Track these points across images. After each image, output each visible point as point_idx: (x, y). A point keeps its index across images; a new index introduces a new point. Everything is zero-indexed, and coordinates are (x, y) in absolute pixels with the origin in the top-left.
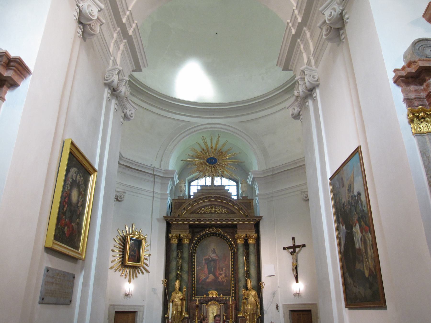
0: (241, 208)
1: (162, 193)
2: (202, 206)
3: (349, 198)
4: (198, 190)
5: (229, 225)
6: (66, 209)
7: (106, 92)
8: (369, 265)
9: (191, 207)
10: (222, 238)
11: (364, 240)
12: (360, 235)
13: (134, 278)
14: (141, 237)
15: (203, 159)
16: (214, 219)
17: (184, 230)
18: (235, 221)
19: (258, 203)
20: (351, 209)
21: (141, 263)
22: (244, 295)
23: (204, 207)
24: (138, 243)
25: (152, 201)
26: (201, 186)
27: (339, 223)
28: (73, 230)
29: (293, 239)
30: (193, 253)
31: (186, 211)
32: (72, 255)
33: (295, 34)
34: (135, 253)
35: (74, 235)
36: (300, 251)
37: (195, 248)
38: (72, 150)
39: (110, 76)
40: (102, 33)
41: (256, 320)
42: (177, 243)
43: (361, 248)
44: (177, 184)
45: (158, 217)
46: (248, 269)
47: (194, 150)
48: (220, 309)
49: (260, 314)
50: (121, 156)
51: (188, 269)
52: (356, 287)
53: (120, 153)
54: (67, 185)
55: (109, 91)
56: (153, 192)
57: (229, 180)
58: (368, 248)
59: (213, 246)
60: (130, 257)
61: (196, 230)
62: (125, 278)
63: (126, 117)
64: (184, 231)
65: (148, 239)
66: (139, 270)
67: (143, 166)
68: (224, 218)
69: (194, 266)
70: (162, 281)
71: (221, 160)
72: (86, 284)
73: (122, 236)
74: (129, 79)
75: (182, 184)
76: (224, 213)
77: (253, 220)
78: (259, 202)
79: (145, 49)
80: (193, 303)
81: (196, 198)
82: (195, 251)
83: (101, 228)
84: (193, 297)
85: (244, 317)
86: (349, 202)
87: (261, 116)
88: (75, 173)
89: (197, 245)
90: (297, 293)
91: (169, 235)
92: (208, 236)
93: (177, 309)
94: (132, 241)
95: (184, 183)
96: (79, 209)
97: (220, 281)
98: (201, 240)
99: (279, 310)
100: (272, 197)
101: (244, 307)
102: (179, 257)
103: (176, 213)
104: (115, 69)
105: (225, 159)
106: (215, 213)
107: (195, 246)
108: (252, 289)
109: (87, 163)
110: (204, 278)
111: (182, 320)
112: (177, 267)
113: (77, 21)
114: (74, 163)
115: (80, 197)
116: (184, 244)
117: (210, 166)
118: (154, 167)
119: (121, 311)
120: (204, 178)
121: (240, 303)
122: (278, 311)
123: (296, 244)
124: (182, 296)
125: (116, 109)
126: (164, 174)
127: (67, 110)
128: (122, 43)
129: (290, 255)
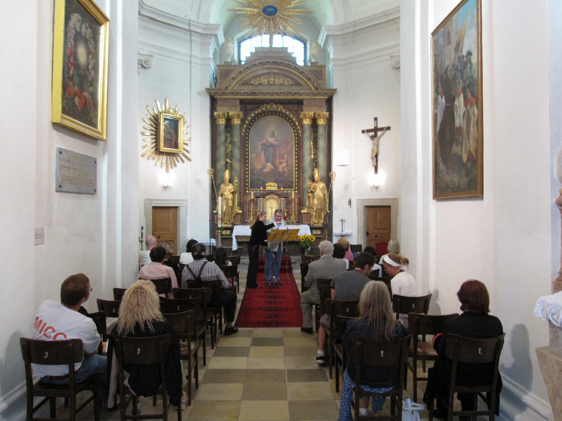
3: (455, 58)
4: (251, 53)
8: (470, 148)
9: (242, 76)
10: (283, 118)
11: (467, 116)
12: (463, 109)
13: (172, 168)
14: (178, 116)
15: (258, 9)
16: (273, 93)
18: (301, 95)
19: (332, 71)
20: (455, 75)
22: (310, 188)
23: (260, 76)
24: (174, 124)
27: (438, 94)
28: (86, 101)
29: (376, 119)
30: (246, 136)
34: (171, 136)
36: (383, 134)
41: (323, 216)
42: (225, 123)
43: (462, 126)
46: (316, 156)
48: (280, 203)
49: (329, 210)
51: (241, 157)
52: (449, 174)
56: (191, 55)
58: (471, 127)
60: (166, 141)
61: (250, 107)
62: (161, 167)
64: (234, 108)
65: (187, 118)
66: (178, 158)
69: (247, 153)
72: (111, 170)
76: (286, 84)
77: (324, 93)
78: (333, 70)
80: (247, 197)
82: (249, 134)
83: (123, 91)
84: (246, 190)
85: (309, 213)
86: (454, 65)
88: (79, 21)
89: (251, 126)
90: (375, 187)
91: (214, 113)
92: (265, 115)
93: (227, 204)
95: (231, 42)
99: (351, 206)
100: (351, 63)
101: (309, 202)
107: (248, 128)
110: (260, 167)
111: (234, 217)
112: (226, 154)
115: (90, 56)
116: (234, 125)
119: (160, 206)
121: (304, 197)
122: (351, 207)
123: (379, 126)
124: (233, 188)
126: (205, 29)
129: (370, 140)
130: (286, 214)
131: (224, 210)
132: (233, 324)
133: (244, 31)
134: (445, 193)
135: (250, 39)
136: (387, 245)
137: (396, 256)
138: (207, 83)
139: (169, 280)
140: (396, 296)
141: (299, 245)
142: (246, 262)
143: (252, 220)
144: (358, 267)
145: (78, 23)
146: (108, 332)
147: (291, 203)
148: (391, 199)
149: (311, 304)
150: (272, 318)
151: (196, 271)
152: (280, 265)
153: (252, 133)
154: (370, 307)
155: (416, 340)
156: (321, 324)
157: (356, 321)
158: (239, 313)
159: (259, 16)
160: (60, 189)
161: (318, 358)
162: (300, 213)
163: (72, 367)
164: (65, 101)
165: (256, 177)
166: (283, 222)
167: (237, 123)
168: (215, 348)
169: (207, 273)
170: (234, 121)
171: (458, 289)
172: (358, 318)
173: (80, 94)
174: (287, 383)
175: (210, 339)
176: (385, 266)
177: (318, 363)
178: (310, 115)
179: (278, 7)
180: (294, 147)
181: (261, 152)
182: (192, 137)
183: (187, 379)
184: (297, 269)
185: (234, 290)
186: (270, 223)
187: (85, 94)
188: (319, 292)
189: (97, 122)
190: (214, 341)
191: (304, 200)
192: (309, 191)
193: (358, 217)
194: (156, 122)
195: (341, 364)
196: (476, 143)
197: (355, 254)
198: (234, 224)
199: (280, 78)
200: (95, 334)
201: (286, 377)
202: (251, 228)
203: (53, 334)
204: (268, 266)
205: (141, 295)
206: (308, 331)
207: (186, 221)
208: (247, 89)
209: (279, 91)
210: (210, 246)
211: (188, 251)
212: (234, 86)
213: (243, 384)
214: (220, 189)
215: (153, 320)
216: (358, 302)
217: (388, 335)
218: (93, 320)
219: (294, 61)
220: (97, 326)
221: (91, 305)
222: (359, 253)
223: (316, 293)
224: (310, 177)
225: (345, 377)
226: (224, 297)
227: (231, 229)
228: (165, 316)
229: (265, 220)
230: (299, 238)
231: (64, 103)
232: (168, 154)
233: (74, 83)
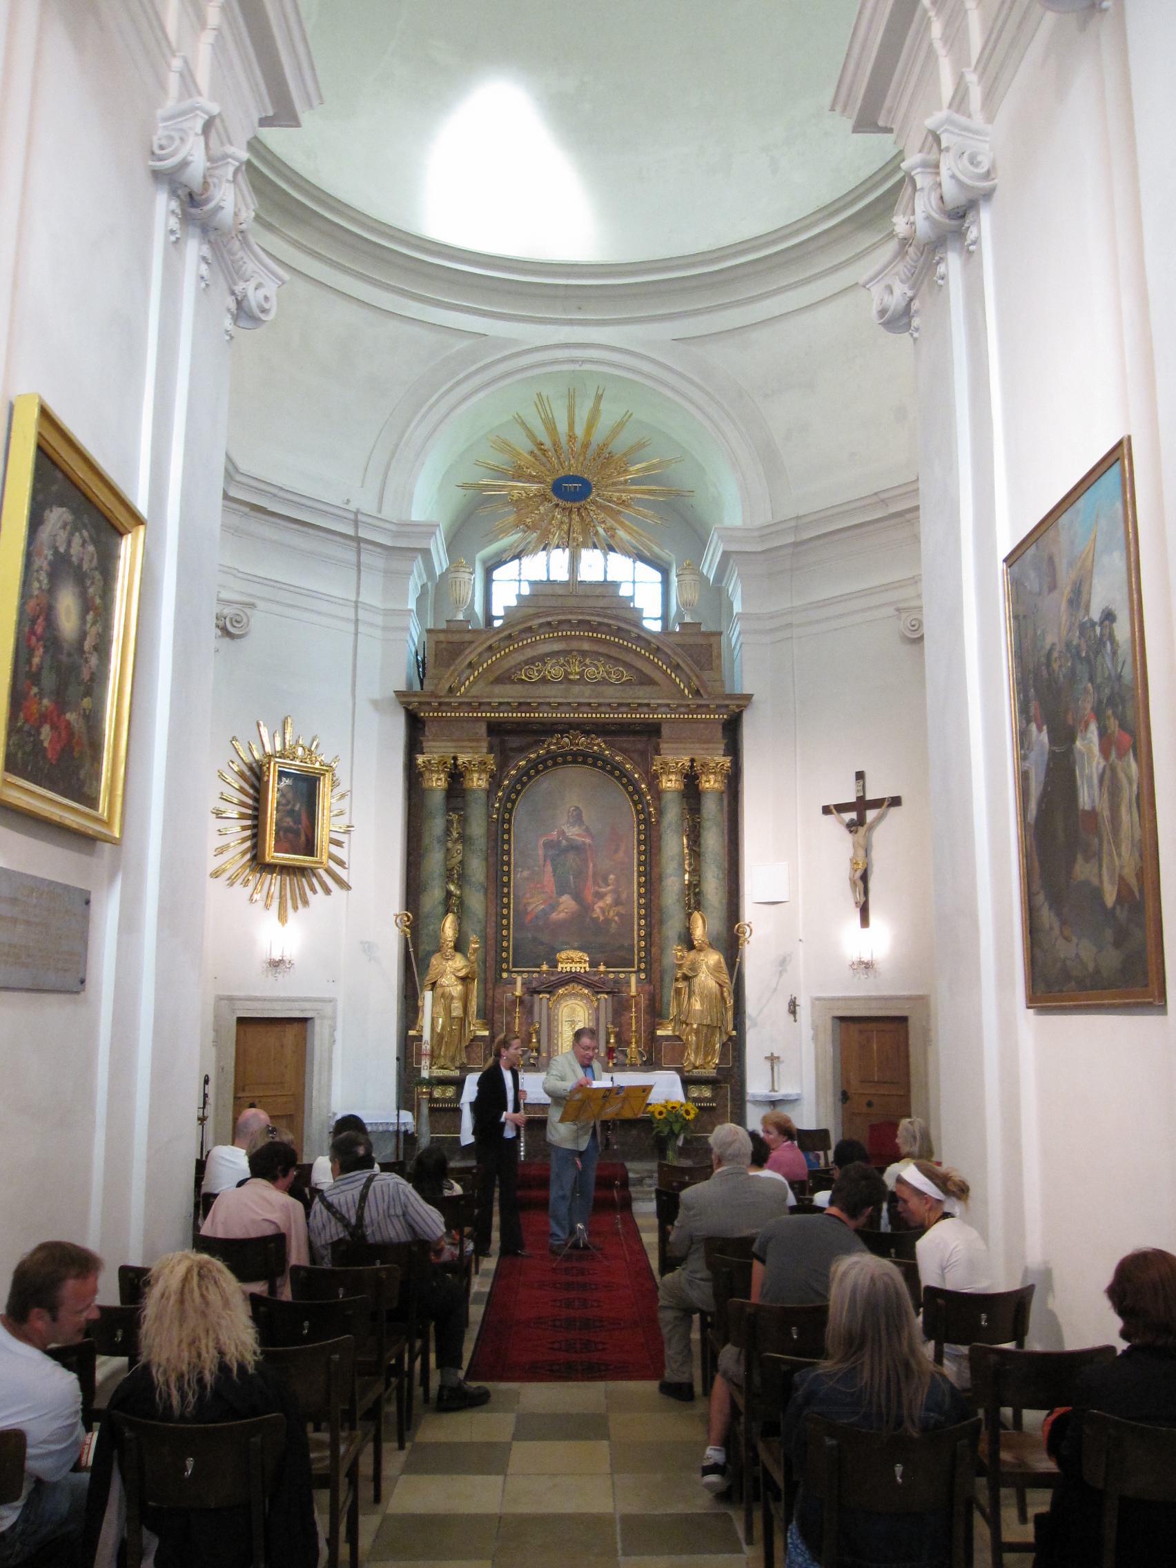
0: (678, 665)
4: (519, 596)
6: (41, 664)
7: (163, 206)
11: (1110, 782)
12: (1098, 763)
13: (296, 908)
14: (317, 765)
16: (580, 704)
18: (654, 711)
19: (738, 647)
20: (1073, 671)
21: (322, 855)
22: (680, 966)
23: (542, 658)
28: (71, 734)
29: (860, 776)
32: (75, 826)
34: (297, 821)
35: (76, 754)
36: (879, 819)
38: (45, 439)
39: (171, 138)
41: (718, 1046)
42: (446, 785)
43: (1098, 809)
46: (697, 878)
47: (504, 446)
49: (735, 1028)
52: (1067, 939)
54: (37, 571)
56: (356, 602)
59: (573, 799)
60: (281, 833)
61: (514, 742)
62: (267, 907)
63: (243, 312)
65: (341, 771)
66: (314, 881)
69: (506, 868)
70: (397, 916)
72: (129, 924)
73: (247, 761)
77: (718, 706)
80: (505, 992)
86: (1068, 645)
88: (64, 527)
89: (518, 793)
92: (555, 764)
93: (448, 1010)
95: (468, 570)
97: (598, 917)
100: (790, 625)
101: (679, 1005)
102: (455, 835)
103: (440, 679)
105: (621, 483)
106: (581, 681)
107: (509, 799)
110: (543, 907)
111: (466, 1047)
114: (54, 488)
115: (90, 617)
116: (474, 791)
117: (564, 509)
121: (665, 991)
122: (795, 1021)
123: (869, 797)
125: (202, 278)
126: (397, 535)
129: (844, 832)
131: (439, 1029)
133: (502, 538)
135: (517, 560)
138: (399, 676)
140: (933, 1292)
145: (61, 532)
148: (909, 998)
149: (687, 1311)
152: (592, 1187)
153: (520, 814)
154: (861, 1346)
155: (995, 1422)
159: (542, 503)
161: (707, 1470)
162: (653, 1040)
164: (15, 738)
168: (408, 1445)
170: (472, 779)
171: (1107, 1276)
173: (56, 719)
174: (621, 1559)
175: (394, 1419)
178: (680, 764)
179: (593, 480)
180: (635, 851)
182: (353, 824)
184: (643, 1200)
187: (71, 716)
189: (99, 792)
190: (405, 1427)
191: (665, 1000)
192: (679, 975)
194: (256, 783)
196: (1137, 855)
199: (599, 664)
201: (619, 1539)
206: (679, 1392)
207: (330, 1059)
208: (510, 693)
210: (398, 1132)
212: (473, 684)
219: (635, 617)
223: (702, 1279)
224: (679, 937)
230: (650, 1108)
231: (11, 743)
232: (285, 870)
233: (41, 690)
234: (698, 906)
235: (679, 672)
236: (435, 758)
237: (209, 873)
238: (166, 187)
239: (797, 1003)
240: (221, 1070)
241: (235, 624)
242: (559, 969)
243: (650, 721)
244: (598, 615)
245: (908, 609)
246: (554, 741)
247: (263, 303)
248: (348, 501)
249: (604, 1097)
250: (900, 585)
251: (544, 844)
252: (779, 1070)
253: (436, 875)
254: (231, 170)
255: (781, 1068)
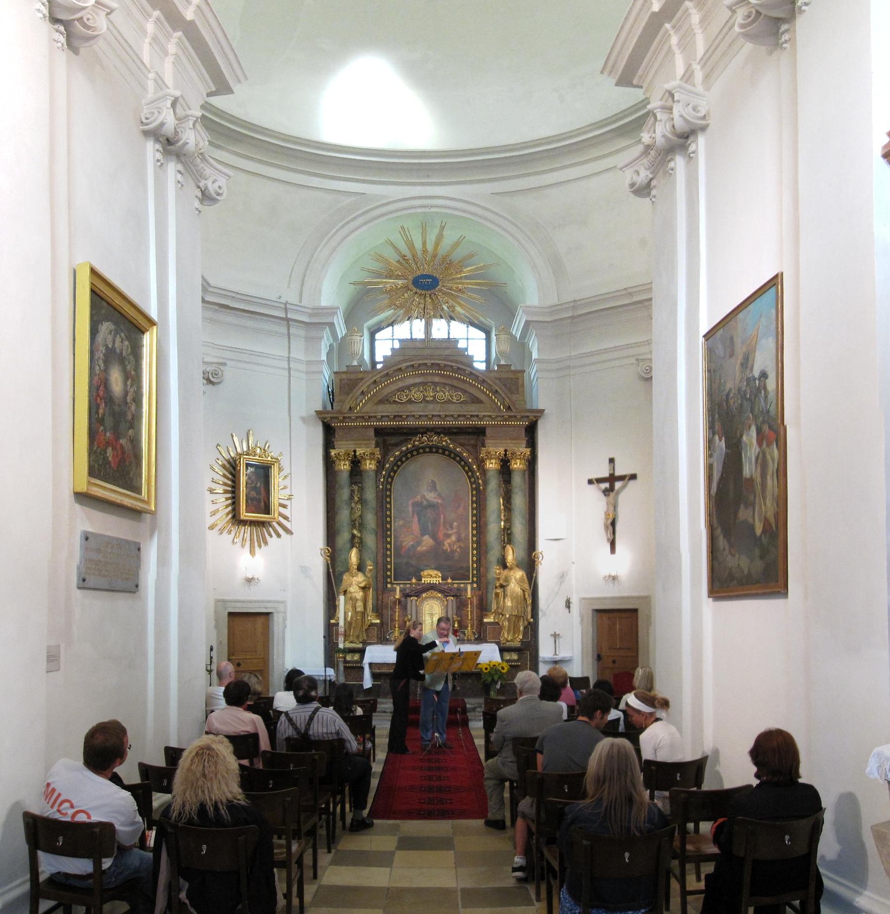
0: (496, 391)
1: (309, 359)
2: (404, 387)
4: (393, 349)
5: (467, 428)
6: (104, 412)
7: (151, 149)
8: (766, 512)
10: (451, 458)
11: (762, 461)
12: (755, 449)
13: (260, 546)
14: (269, 459)
17: (364, 440)
18: (481, 419)
19: (535, 380)
20: (741, 405)
21: (274, 514)
22: (498, 579)
23: (408, 388)
24: (263, 473)
25: (287, 378)
26: (401, 341)
28: (123, 453)
29: (612, 461)
30: (387, 490)
31: (366, 398)
32: (129, 505)
33: (659, 11)
34: (259, 493)
35: (127, 464)
36: (624, 487)
37: (390, 480)
38: (94, 285)
39: (153, 113)
40: (116, 28)
41: (522, 628)
43: (754, 477)
44: (343, 337)
45: (304, 413)
46: (509, 524)
47: (380, 258)
48: (447, 606)
49: (532, 617)
50: (205, 284)
51: (377, 526)
52: (733, 555)
53: (203, 277)
54: (97, 360)
55: (158, 146)
56: (289, 357)
57: (468, 327)
58: (769, 477)
59: (430, 475)
60: (249, 501)
61: (392, 440)
62: (243, 546)
63: (206, 197)
64: (365, 442)
65: (285, 462)
66: (271, 529)
67: (259, 301)
68: (455, 413)
69: (388, 519)
70: (321, 550)
71: (449, 281)
72: (163, 561)
73: (227, 458)
74: (203, 114)
75: (354, 338)
77: (522, 417)
79: (234, 44)
80: (389, 596)
81: (389, 368)
82: (391, 486)
85: (498, 623)
86: (739, 390)
87: (553, 183)
89: (395, 472)
91: (330, 452)
92: (418, 453)
93: (354, 607)
94: (249, 468)
95: (359, 335)
96: (129, 409)
97: (447, 550)
98: (402, 462)
100: (569, 367)
101: (498, 603)
102: (356, 499)
103: (344, 402)
104: (164, 97)
105: (458, 279)
106: (434, 401)
107: (389, 476)
108: (515, 567)
109: (133, 310)
110: (412, 543)
111: (366, 630)
112: (352, 521)
113: (47, 18)
114: (103, 311)
115: (129, 383)
116: (366, 471)
118: (287, 302)
119: (240, 611)
120: (407, 323)
121: (489, 595)
122: (569, 612)
125: (179, 182)
126: (311, 315)
127: (69, 203)
128: (172, 40)
129: (602, 495)
130: (456, 625)
132: (365, 812)
134: (728, 586)
136: (632, 676)
137: (647, 695)
138: (318, 402)
139: (255, 737)
140: (649, 763)
141: (481, 678)
142: (386, 708)
143: (397, 635)
144: (583, 716)
146: (156, 817)
147: (466, 606)
148: (638, 598)
150: (434, 804)
151: (301, 724)
152: (447, 713)
153: (397, 484)
154: (604, 782)
156: (519, 814)
157: (581, 806)
158: (375, 795)
160: (83, 584)
161: (515, 870)
162: (481, 624)
163: (97, 864)
165: (405, 561)
166: (452, 638)
167: (371, 468)
168: (333, 851)
169: (320, 727)
171: (750, 744)
172: (584, 801)
173: (114, 443)
176: (630, 712)
177: (514, 877)
180: (470, 508)
181: (413, 517)
183: (285, 898)
184: (476, 720)
185: (366, 756)
186: (429, 641)
187: (123, 441)
188: (515, 760)
190: (331, 842)
191: (489, 601)
193: (582, 630)
195: (555, 877)
196: (775, 505)
197: (578, 693)
198: (365, 643)
200: (135, 817)
201: (460, 900)
202: (396, 650)
203: (71, 812)
204: (425, 715)
205: (209, 760)
206: (497, 825)
207: (284, 637)
209: (444, 414)
210: (325, 681)
211: (287, 689)
212: (364, 405)
213: (382, 910)
214: (341, 581)
215: (229, 801)
216: (584, 774)
217: (636, 827)
218: (132, 795)
220: (137, 805)
221: (128, 771)
222: (584, 691)
223: (511, 762)
224: (498, 560)
225: (563, 897)
226: (349, 768)
227: (362, 652)
228: (248, 797)
229: (421, 636)
230: (479, 666)
234: (510, 542)
235: (496, 395)
236: (342, 451)
237: (207, 528)
238: (152, 138)
239: (571, 601)
240: (220, 643)
241: (215, 376)
242: (423, 582)
243: (479, 426)
244: (444, 360)
245: (645, 359)
246: (418, 439)
247: (218, 190)
248: (280, 297)
249: (451, 658)
250: (637, 345)
251: (412, 504)
252: (559, 642)
253: (345, 524)
254: (191, 123)
255: (560, 641)
